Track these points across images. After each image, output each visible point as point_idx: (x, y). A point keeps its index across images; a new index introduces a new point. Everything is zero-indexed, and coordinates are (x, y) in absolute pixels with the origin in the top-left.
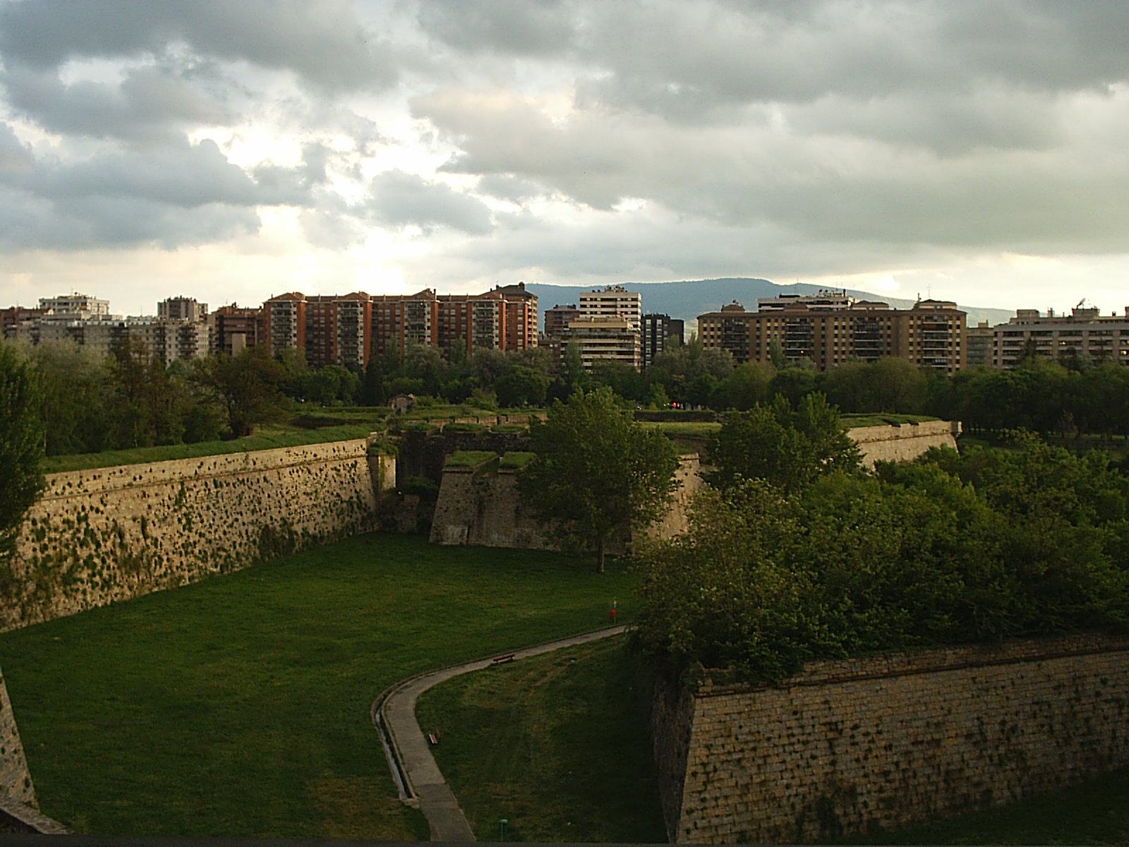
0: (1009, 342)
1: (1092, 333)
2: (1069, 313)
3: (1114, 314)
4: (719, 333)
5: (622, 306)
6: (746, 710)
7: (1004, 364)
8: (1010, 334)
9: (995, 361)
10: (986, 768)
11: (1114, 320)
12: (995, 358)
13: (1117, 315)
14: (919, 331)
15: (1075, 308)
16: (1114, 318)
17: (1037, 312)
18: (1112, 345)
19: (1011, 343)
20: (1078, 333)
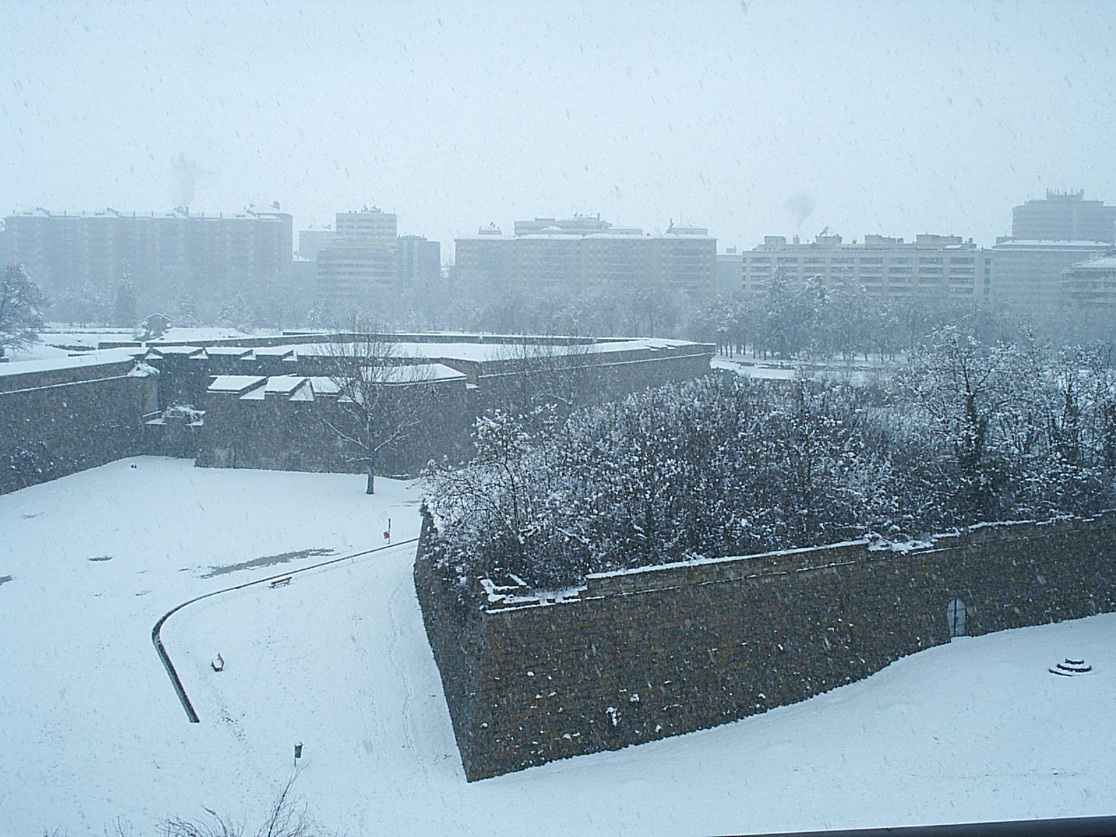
0: (757, 267)
1: (835, 260)
2: (812, 241)
3: (854, 242)
4: (476, 255)
5: (378, 228)
6: (1048, 405)
7: (889, 281)
8: (758, 260)
9: (744, 286)
10: (908, 560)
11: (854, 248)
12: (743, 283)
13: (858, 242)
14: (671, 256)
15: (819, 235)
16: (854, 246)
17: (784, 239)
18: (882, 272)
19: (758, 269)
20: (880, 261)
